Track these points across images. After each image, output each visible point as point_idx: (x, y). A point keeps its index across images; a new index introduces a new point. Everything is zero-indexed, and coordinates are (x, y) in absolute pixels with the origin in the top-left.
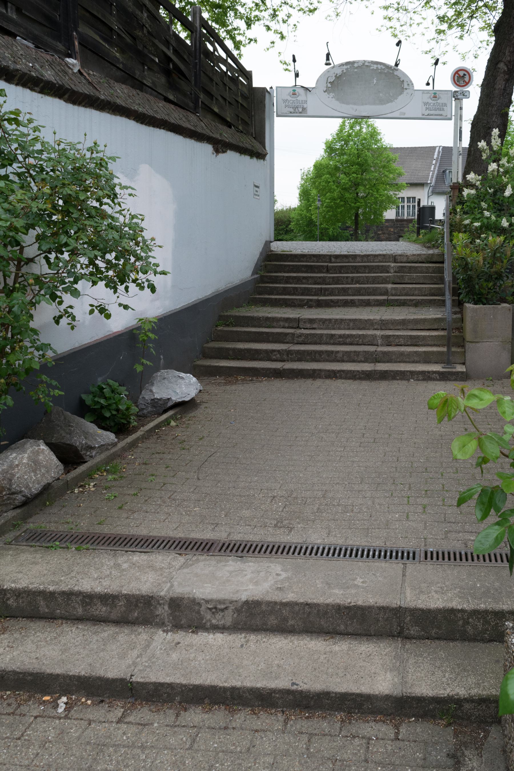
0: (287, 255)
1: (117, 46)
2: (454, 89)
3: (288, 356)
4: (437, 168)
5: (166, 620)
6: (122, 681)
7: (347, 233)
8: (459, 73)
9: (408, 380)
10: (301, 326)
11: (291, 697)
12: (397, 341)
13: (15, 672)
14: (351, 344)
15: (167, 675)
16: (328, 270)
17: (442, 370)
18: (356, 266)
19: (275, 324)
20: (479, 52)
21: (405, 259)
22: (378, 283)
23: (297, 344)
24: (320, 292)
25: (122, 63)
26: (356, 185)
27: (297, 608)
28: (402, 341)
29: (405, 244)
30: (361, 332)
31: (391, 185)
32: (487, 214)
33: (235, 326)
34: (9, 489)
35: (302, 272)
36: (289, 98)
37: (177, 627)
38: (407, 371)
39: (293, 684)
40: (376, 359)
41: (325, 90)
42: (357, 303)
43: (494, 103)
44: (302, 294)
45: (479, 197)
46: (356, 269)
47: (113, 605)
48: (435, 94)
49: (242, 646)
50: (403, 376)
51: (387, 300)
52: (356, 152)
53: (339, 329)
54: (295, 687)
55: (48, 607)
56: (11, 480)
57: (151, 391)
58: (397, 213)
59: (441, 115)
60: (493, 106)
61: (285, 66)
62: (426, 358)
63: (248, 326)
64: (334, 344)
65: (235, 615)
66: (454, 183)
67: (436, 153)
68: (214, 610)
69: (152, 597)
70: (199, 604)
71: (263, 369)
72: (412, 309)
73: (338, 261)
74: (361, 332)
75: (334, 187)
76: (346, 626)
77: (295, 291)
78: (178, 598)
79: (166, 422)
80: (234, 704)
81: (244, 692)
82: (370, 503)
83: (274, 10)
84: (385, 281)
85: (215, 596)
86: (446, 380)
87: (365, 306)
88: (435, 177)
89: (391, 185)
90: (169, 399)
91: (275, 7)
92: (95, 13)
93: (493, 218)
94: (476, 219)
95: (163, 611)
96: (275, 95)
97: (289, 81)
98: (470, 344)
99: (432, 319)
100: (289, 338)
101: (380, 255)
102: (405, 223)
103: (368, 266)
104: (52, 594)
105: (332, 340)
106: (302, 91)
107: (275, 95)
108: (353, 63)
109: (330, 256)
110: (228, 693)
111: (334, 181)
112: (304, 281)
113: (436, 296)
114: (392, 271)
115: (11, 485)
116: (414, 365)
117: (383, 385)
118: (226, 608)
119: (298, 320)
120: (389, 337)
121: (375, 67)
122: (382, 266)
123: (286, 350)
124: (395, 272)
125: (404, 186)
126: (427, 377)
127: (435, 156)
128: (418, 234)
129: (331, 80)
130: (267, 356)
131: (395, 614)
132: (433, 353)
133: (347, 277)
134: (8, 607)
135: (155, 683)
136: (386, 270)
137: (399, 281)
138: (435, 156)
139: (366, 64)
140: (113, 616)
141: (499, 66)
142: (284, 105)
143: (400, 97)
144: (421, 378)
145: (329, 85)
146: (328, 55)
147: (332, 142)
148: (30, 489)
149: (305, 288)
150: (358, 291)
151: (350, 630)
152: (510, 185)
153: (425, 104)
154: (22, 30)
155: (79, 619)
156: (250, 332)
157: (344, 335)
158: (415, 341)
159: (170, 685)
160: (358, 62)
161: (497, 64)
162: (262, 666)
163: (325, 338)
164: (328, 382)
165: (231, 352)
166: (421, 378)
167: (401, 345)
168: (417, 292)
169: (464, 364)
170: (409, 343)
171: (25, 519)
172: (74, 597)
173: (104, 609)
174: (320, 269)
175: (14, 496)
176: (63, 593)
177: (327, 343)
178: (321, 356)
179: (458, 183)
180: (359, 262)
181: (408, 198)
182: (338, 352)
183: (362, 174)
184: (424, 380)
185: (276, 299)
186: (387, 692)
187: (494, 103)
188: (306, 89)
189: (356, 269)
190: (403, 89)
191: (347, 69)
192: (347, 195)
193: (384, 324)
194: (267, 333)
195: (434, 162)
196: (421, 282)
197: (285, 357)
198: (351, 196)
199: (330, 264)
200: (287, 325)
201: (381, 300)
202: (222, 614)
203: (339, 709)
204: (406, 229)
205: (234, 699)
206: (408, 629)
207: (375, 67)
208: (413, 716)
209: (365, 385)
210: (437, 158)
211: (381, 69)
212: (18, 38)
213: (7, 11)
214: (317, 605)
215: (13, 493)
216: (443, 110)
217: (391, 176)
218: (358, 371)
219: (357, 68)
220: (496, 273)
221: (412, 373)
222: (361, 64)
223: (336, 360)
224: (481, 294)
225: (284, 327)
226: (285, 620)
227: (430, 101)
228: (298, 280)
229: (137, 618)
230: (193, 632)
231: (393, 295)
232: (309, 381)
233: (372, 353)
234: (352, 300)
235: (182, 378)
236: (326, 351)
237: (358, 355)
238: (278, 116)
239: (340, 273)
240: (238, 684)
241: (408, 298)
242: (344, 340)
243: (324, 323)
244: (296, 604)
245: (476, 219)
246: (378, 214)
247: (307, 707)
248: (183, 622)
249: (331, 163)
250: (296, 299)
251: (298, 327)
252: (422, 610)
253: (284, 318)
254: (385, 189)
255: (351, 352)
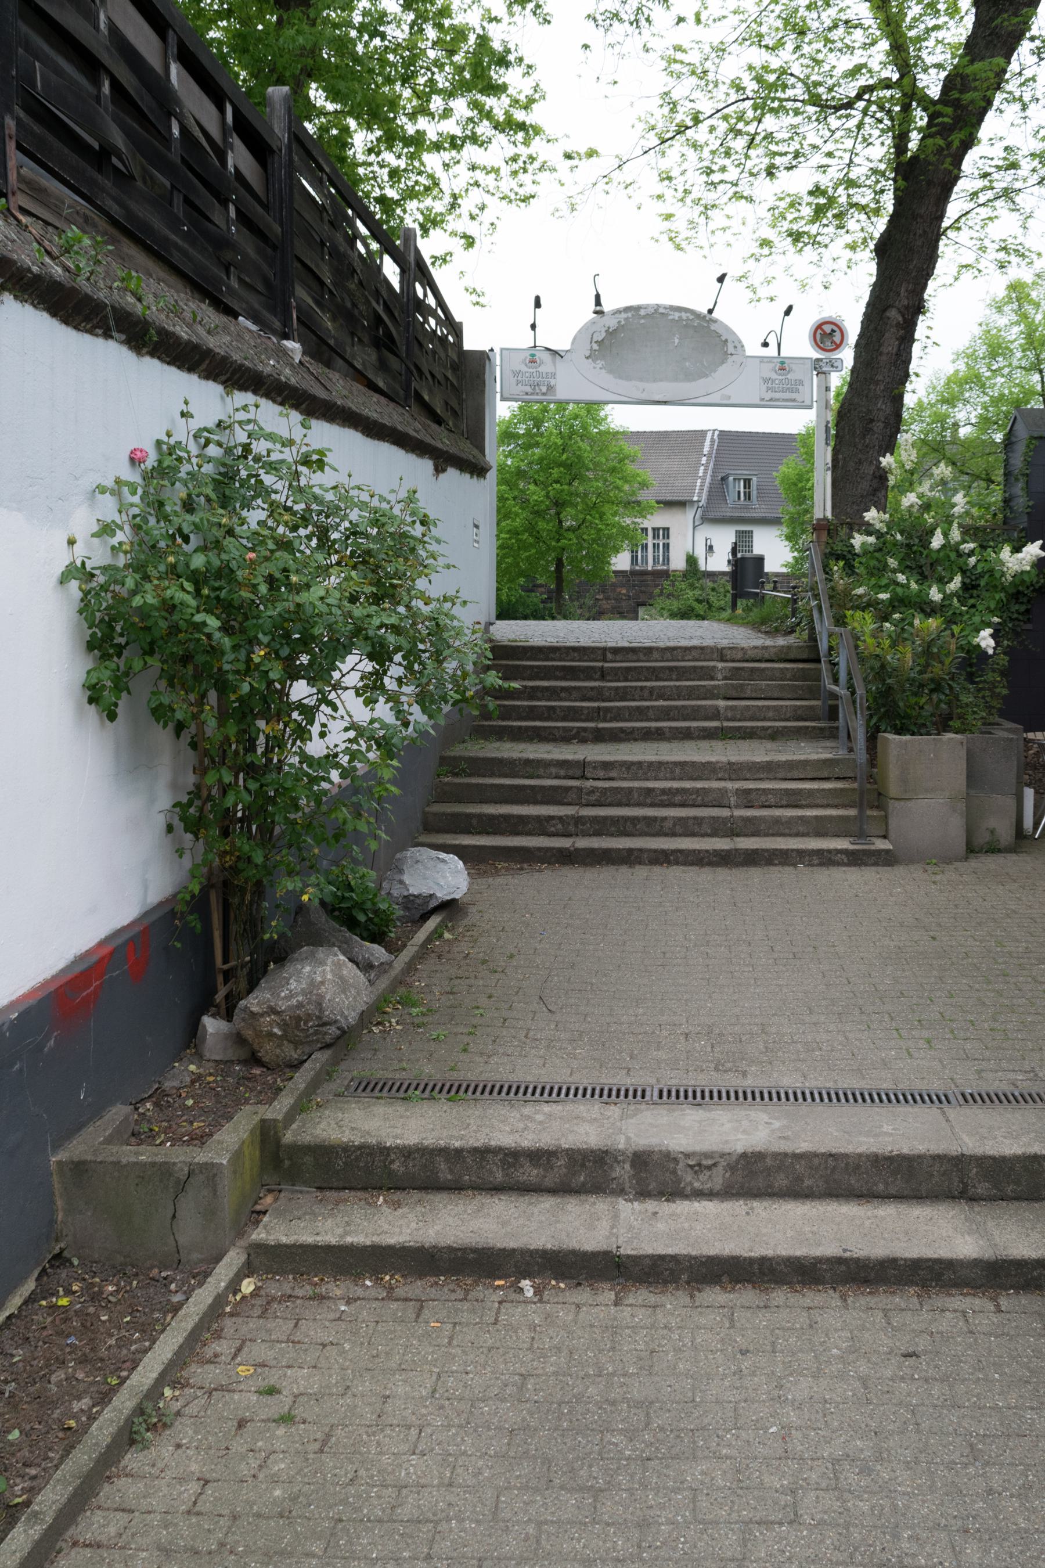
0: (524, 647)
1: (329, 310)
2: (815, 354)
3: (576, 826)
4: (710, 472)
5: (627, 1185)
6: (606, 1254)
7: (536, 598)
8: (825, 327)
9: (795, 865)
10: (588, 774)
11: (843, 1268)
12: (763, 798)
13: (450, 1249)
14: (683, 805)
15: (666, 1246)
16: (603, 674)
17: (852, 847)
18: (654, 668)
19: (541, 771)
20: (832, 278)
21: (739, 656)
22: (698, 698)
23: (587, 805)
24: (598, 714)
25: (336, 339)
26: (559, 504)
27: (816, 1161)
28: (772, 800)
29: (715, 625)
30: (699, 785)
31: (628, 504)
32: (901, 578)
33: (470, 775)
34: (319, 1018)
35: (557, 679)
36: (524, 369)
37: (643, 1194)
38: (793, 850)
39: (845, 1250)
40: (732, 830)
41: (588, 353)
42: (668, 735)
43: (880, 377)
44: (564, 719)
45: (882, 548)
46: (655, 674)
47: (549, 1166)
48: (783, 363)
49: (748, 1213)
50: (802, 856)
51: (722, 728)
52: (559, 442)
53: (656, 779)
54: (848, 1254)
55: (451, 1171)
56: (320, 1004)
57: (401, 882)
58: (634, 560)
59: (794, 400)
60: (877, 383)
61: (474, 298)
62: (820, 828)
63: (492, 775)
64: (653, 805)
65: (727, 1175)
66: (818, 520)
67: (707, 443)
68: (698, 1168)
69: (606, 1152)
70: (676, 1160)
71: (539, 849)
72: (769, 745)
73: (618, 658)
74: (699, 785)
75: (517, 509)
76: (887, 1184)
77: (550, 714)
78: (644, 1152)
79: (436, 934)
80: (763, 1281)
81: (778, 1264)
82: (841, 1038)
83: (455, 197)
84: (710, 694)
85: (698, 1148)
86: (860, 865)
87: (682, 739)
88: (706, 488)
89: (628, 504)
90: (431, 896)
91: (457, 191)
92: (308, 262)
93: (914, 586)
94: (880, 587)
95: (623, 1172)
96: (498, 362)
97: (525, 340)
98: (896, 804)
99: (818, 761)
100: (572, 796)
101: (695, 648)
102: (649, 578)
103: (676, 668)
104: (459, 1152)
105: (648, 798)
106: (546, 357)
107: (498, 362)
108: (638, 308)
109: (604, 650)
110: (756, 1266)
111: (514, 498)
112: (563, 695)
113: (806, 720)
114: (720, 676)
115: (321, 1011)
116: (799, 839)
117: (755, 875)
118: (715, 1165)
119: (583, 764)
120: (748, 792)
121: (676, 315)
122: (702, 667)
123: (573, 817)
124: (725, 678)
125: (653, 507)
126: (826, 859)
127: (706, 449)
128: (734, 606)
129: (599, 337)
130: (540, 826)
131: (956, 1165)
132: (830, 818)
133: (642, 688)
134: (391, 1174)
135: (653, 1256)
136: (708, 674)
137: (735, 695)
138: (706, 449)
139: (661, 310)
140: (548, 1182)
141: (888, 314)
142: (514, 381)
143: (722, 369)
144: (816, 862)
145: (595, 347)
146: (598, 297)
147: (510, 422)
148: (346, 1018)
149: (569, 708)
150: (666, 714)
151: (893, 1191)
152: (939, 530)
153: (766, 380)
154: (244, 306)
155: (497, 1189)
156: (502, 786)
157: (670, 789)
158: (793, 800)
159: (674, 1258)
160: (646, 307)
161: (884, 311)
162: (790, 1233)
163: (636, 796)
164: (657, 869)
165: (474, 821)
166: (816, 862)
167: (770, 807)
168: (770, 714)
169: (885, 837)
170: (784, 803)
171: (336, 1062)
172: (491, 1156)
173: (535, 1172)
174: (587, 674)
175: (324, 1029)
176: (475, 1150)
177: (639, 805)
178: (635, 825)
179: (825, 519)
180: (656, 661)
181: (654, 529)
182: (664, 819)
183: (570, 484)
184: (821, 864)
185: (520, 727)
186: (975, 1256)
187: (880, 378)
188: (555, 353)
189: (655, 674)
190: (726, 355)
191: (626, 319)
192: (542, 525)
193: (734, 771)
194: (532, 788)
195: (704, 460)
196: (776, 695)
197: (572, 828)
198: (550, 527)
199: (606, 665)
200: (562, 773)
201: (710, 728)
202: (708, 1173)
203: (911, 1283)
204: (657, 591)
205: (764, 1274)
206: (974, 1186)
207: (676, 315)
208: (1011, 1287)
209: (723, 874)
210: (710, 453)
211: (688, 319)
212: (241, 318)
213: (229, 278)
214: (846, 1156)
215: (325, 1024)
216: (798, 391)
217: (626, 487)
218: (707, 851)
219: (644, 317)
220: (932, 680)
221: (801, 853)
222: (651, 311)
223: (661, 833)
224: (908, 717)
225: (557, 777)
226: (799, 1179)
227: (774, 376)
228: (553, 693)
229: (584, 1184)
230: (667, 1200)
231: (728, 720)
232: (624, 869)
233: (725, 820)
234: (658, 729)
235: (443, 861)
236: (645, 818)
237: (700, 825)
238: (503, 399)
239: (626, 680)
240: (770, 1253)
241: (760, 724)
242: (669, 798)
243: (628, 768)
244: (816, 1155)
245: (880, 587)
246: (601, 559)
247: (866, 1282)
248: (651, 1187)
249: (509, 463)
250: (558, 728)
251: (583, 777)
252: (993, 1158)
253: (557, 761)
254: (615, 514)
255: (688, 818)
